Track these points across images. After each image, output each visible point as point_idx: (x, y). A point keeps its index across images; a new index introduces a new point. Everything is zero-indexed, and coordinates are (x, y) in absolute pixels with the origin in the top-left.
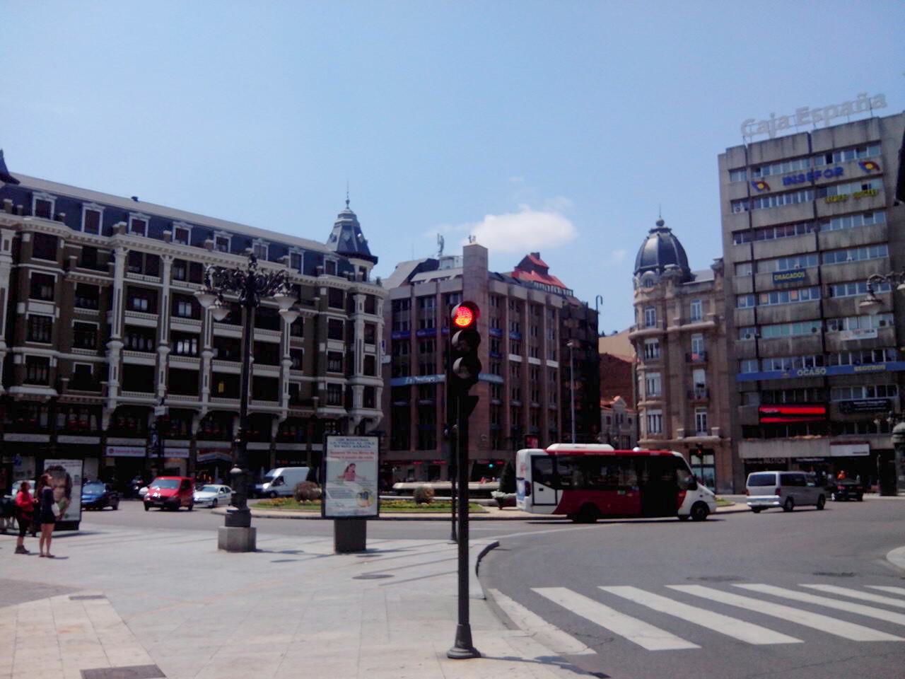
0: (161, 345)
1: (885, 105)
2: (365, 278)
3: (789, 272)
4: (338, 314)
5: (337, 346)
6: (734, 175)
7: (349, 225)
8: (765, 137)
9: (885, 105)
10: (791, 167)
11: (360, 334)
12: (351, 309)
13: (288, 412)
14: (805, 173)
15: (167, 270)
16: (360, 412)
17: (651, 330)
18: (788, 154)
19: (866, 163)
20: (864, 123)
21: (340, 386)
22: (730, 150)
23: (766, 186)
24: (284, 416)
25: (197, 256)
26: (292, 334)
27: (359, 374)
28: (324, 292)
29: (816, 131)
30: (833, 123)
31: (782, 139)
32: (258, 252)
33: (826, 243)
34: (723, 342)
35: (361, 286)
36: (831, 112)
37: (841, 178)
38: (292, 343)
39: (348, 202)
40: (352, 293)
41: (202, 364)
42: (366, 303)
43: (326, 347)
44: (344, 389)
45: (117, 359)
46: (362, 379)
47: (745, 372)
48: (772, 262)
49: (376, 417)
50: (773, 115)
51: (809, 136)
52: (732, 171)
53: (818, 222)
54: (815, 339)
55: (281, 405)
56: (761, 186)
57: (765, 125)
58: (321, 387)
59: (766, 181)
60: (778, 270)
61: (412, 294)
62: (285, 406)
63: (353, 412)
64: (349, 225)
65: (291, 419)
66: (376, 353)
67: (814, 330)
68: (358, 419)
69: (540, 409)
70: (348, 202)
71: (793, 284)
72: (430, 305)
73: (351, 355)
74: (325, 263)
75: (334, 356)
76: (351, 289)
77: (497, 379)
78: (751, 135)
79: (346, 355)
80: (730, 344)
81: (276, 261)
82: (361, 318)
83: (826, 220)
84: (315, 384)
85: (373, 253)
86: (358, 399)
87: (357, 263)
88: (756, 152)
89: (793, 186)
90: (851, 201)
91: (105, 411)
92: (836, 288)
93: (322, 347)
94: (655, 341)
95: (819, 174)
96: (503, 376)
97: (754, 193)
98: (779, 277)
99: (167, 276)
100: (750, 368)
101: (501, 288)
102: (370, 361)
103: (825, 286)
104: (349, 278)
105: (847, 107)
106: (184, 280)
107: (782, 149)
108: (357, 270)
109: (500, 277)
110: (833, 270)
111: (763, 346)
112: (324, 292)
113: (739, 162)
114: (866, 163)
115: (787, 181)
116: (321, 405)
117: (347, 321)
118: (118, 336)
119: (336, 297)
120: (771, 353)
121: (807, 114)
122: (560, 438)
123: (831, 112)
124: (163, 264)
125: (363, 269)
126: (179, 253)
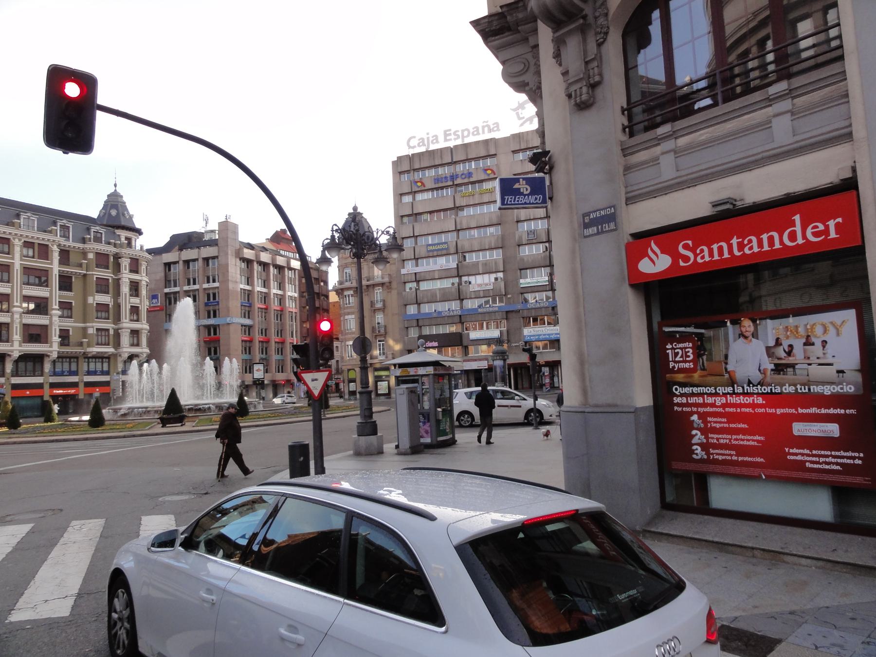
0: (15, 306)
1: (498, 130)
2: (129, 244)
4: (107, 274)
6: (402, 176)
7: (114, 202)
8: (423, 149)
9: (498, 130)
10: (441, 171)
11: (125, 289)
12: (117, 268)
13: (59, 352)
14: (448, 176)
15: (17, 250)
16: (126, 349)
17: (348, 284)
19: (486, 170)
21: (108, 330)
22: (399, 158)
24: (55, 355)
25: (43, 239)
26: (60, 289)
27: (125, 320)
28: (91, 256)
29: (456, 146)
33: (461, 223)
34: (394, 292)
35: (125, 251)
36: (466, 133)
37: (472, 180)
38: (60, 297)
40: (117, 257)
41: (12, 317)
42: (130, 265)
44: (111, 332)
45: (18, 321)
46: (127, 324)
47: (408, 313)
49: (142, 353)
51: (451, 149)
52: (400, 173)
53: (457, 208)
54: (453, 290)
55: (51, 346)
58: (91, 331)
62: (16, 345)
63: (120, 350)
64: (114, 202)
65: (61, 357)
66: (141, 303)
67: (453, 284)
68: (126, 356)
69: (283, 342)
73: (118, 306)
74: (92, 233)
75: (102, 308)
76: (117, 254)
77: (247, 322)
78: (414, 147)
79: (114, 306)
80: (399, 294)
82: (126, 276)
83: (461, 208)
84: (85, 329)
85: (138, 226)
86: (125, 339)
87: (123, 234)
88: (416, 160)
89: (440, 185)
90: (477, 196)
92: (467, 255)
93: (90, 300)
94: (351, 292)
95: (457, 176)
96: (253, 319)
97: (415, 189)
98: (431, 248)
99: (17, 255)
100: (412, 310)
102: (135, 310)
103: (460, 252)
104: (115, 245)
105: (477, 130)
106: (33, 257)
108: (123, 239)
110: (465, 244)
111: (420, 295)
112: (91, 256)
114: (486, 170)
115: (437, 180)
116: (89, 345)
117: (114, 279)
118: (57, 307)
119: (102, 260)
120: (426, 300)
121: (450, 134)
124: (14, 245)
125: (129, 240)
126: (27, 236)
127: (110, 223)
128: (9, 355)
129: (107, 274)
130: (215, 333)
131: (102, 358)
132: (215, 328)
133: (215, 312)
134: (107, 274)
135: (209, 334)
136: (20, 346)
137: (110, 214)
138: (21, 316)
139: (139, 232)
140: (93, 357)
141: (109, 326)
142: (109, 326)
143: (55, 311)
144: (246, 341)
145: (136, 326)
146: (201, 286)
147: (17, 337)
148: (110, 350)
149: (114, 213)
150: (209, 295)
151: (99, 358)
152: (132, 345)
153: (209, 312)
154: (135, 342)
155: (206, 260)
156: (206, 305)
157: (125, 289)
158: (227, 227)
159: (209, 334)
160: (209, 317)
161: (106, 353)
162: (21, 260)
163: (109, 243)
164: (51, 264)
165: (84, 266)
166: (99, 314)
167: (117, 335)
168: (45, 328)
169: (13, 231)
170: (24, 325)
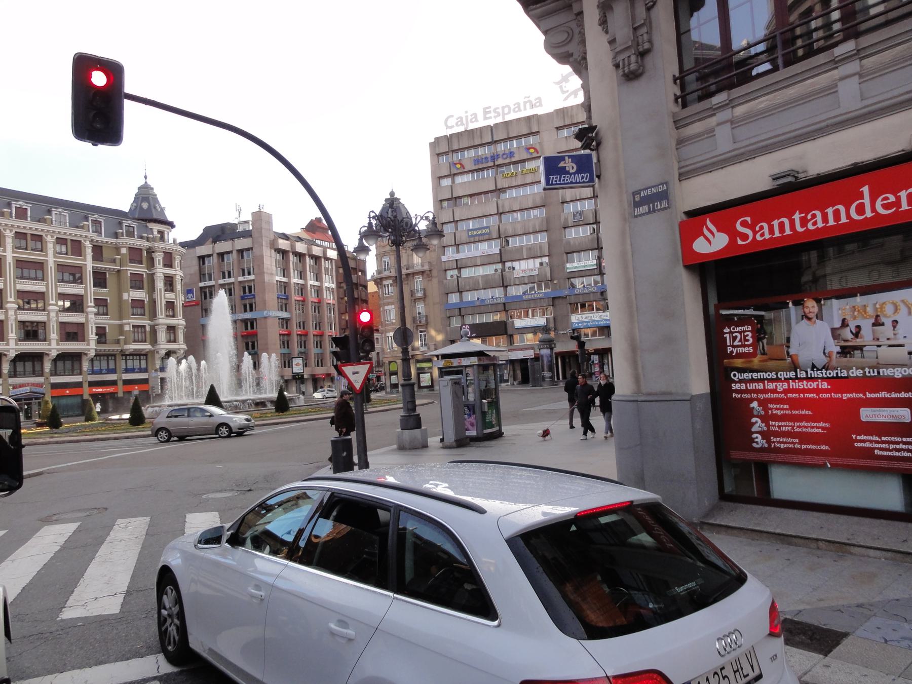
1: (541, 105)
2: (162, 238)
3: (479, 229)
5: (140, 295)
6: (440, 158)
7: (145, 195)
8: (461, 129)
9: (541, 105)
10: (481, 151)
11: (160, 284)
12: (151, 263)
13: (96, 350)
14: (489, 156)
15: (50, 246)
17: (386, 273)
18: (477, 142)
19: (529, 149)
20: (528, 119)
21: (144, 327)
22: (437, 139)
23: (462, 166)
25: (36, 229)
26: (95, 286)
28: (124, 251)
29: (496, 125)
30: (508, 118)
31: (472, 130)
32: (763, 57)
35: (158, 245)
36: (506, 110)
37: (513, 160)
39: (146, 177)
40: (150, 251)
42: (164, 259)
43: (129, 296)
44: (148, 329)
46: (163, 320)
48: (467, 222)
49: (179, 349)
50: (466, 112)
52: (438, 155)
53: (499, 191)
55: (8, 344)
56: (458, 166)
57: (460, 121)
58: (127, 328)
59: (463, 163)
60: (471, 227)
61: (213, 251)
63: (158, 347)
64: (145, 195)
66: (176, 299)
67: (496, 270)
70: (146, 177)
71: (481, 238)
72: (248, 256)
75: (137, 304)
76: (150, 248)
77: (285, 315)
79: (149, 302)
81: (77, 227)
82: (160, 271)
84: (121, 327)
85: (170, 218)
86: (162, 336)
87: (156, 227)
89: (481, 166)
90: (519, 177)
91: (157, 356)
92: (510, 240)
93: (125, 296)
94: (390, 282)
96: (291, 312)
97: (454, 171)
98: (472, 233)
99: (51, 253)
100: (454, 298)
101: (283, 244)
102: (170, 305)
103: (503, 237)
104: (148, 239)
106: (67, 254)
107: (473, 138)
108: (155, 233)
109: (285, 237)
112: (124, 251)
113: (444, 148)
114: (529, 149)
115: (477, 161)
117: (148, 274)
119: (135, 255)
120: (468, 288)
121: (490, 112)
122: (353, 357)
123: (506, 110)
125: (161, 233)
126: (18, 227)
127: (142, 217)
128: (48, 355)
129: (141, 269)
130: (252, 327)
131: (140, 355)
132: (252, 322)
133: (251, 306)
134: (141, 269)
135: (246, 328)
136: (58, 344)
137: (141, 207)
138: (57, 314)
139: (171, 225)
140: (132, 355)
141: (145, 322)
142: (145, 322)
143: (91, 309)
144: (283, 335)
145: (172, 321)
146: (236, 279)
147: (54, 335)
148: (147, 347)
149: (145, 205)
150: (244, 288)
151: (136, 355)
152: (169, 341)
153: (245, 306)
154: (172, 338)
155: (241, 252)
156: (242, 298)
157: (160, 284)
158: (260, 217)
159: (246, 328)
160: (245, 311)
161: (143, 350)
162: (55, 257)
163: (142, 237)
164: (85, 260)
165: (118, 261)
166: (135, 311)
167: (154, 332)
168: (81, 326)
169: (46, 228)
170: (61, 323)
